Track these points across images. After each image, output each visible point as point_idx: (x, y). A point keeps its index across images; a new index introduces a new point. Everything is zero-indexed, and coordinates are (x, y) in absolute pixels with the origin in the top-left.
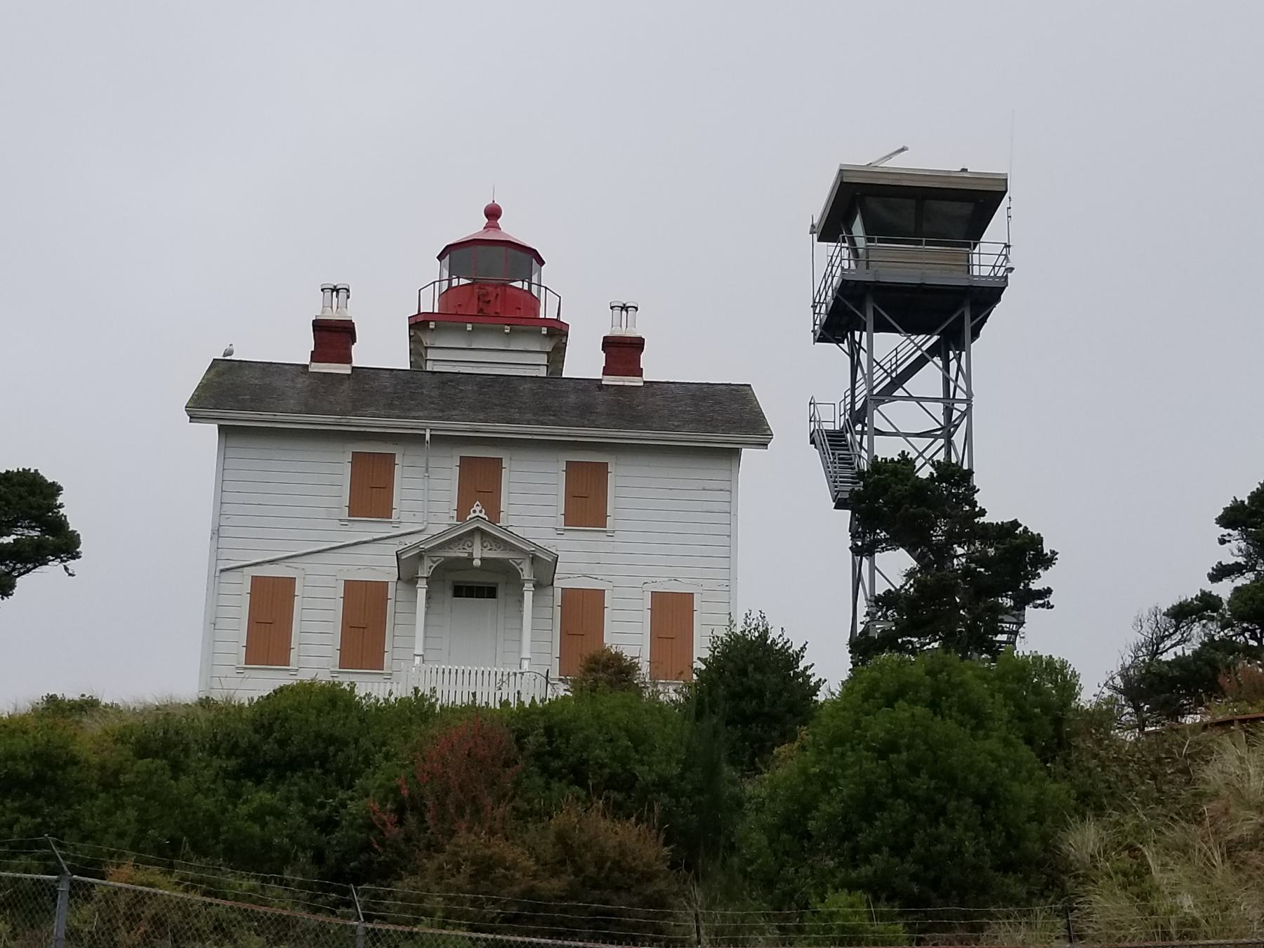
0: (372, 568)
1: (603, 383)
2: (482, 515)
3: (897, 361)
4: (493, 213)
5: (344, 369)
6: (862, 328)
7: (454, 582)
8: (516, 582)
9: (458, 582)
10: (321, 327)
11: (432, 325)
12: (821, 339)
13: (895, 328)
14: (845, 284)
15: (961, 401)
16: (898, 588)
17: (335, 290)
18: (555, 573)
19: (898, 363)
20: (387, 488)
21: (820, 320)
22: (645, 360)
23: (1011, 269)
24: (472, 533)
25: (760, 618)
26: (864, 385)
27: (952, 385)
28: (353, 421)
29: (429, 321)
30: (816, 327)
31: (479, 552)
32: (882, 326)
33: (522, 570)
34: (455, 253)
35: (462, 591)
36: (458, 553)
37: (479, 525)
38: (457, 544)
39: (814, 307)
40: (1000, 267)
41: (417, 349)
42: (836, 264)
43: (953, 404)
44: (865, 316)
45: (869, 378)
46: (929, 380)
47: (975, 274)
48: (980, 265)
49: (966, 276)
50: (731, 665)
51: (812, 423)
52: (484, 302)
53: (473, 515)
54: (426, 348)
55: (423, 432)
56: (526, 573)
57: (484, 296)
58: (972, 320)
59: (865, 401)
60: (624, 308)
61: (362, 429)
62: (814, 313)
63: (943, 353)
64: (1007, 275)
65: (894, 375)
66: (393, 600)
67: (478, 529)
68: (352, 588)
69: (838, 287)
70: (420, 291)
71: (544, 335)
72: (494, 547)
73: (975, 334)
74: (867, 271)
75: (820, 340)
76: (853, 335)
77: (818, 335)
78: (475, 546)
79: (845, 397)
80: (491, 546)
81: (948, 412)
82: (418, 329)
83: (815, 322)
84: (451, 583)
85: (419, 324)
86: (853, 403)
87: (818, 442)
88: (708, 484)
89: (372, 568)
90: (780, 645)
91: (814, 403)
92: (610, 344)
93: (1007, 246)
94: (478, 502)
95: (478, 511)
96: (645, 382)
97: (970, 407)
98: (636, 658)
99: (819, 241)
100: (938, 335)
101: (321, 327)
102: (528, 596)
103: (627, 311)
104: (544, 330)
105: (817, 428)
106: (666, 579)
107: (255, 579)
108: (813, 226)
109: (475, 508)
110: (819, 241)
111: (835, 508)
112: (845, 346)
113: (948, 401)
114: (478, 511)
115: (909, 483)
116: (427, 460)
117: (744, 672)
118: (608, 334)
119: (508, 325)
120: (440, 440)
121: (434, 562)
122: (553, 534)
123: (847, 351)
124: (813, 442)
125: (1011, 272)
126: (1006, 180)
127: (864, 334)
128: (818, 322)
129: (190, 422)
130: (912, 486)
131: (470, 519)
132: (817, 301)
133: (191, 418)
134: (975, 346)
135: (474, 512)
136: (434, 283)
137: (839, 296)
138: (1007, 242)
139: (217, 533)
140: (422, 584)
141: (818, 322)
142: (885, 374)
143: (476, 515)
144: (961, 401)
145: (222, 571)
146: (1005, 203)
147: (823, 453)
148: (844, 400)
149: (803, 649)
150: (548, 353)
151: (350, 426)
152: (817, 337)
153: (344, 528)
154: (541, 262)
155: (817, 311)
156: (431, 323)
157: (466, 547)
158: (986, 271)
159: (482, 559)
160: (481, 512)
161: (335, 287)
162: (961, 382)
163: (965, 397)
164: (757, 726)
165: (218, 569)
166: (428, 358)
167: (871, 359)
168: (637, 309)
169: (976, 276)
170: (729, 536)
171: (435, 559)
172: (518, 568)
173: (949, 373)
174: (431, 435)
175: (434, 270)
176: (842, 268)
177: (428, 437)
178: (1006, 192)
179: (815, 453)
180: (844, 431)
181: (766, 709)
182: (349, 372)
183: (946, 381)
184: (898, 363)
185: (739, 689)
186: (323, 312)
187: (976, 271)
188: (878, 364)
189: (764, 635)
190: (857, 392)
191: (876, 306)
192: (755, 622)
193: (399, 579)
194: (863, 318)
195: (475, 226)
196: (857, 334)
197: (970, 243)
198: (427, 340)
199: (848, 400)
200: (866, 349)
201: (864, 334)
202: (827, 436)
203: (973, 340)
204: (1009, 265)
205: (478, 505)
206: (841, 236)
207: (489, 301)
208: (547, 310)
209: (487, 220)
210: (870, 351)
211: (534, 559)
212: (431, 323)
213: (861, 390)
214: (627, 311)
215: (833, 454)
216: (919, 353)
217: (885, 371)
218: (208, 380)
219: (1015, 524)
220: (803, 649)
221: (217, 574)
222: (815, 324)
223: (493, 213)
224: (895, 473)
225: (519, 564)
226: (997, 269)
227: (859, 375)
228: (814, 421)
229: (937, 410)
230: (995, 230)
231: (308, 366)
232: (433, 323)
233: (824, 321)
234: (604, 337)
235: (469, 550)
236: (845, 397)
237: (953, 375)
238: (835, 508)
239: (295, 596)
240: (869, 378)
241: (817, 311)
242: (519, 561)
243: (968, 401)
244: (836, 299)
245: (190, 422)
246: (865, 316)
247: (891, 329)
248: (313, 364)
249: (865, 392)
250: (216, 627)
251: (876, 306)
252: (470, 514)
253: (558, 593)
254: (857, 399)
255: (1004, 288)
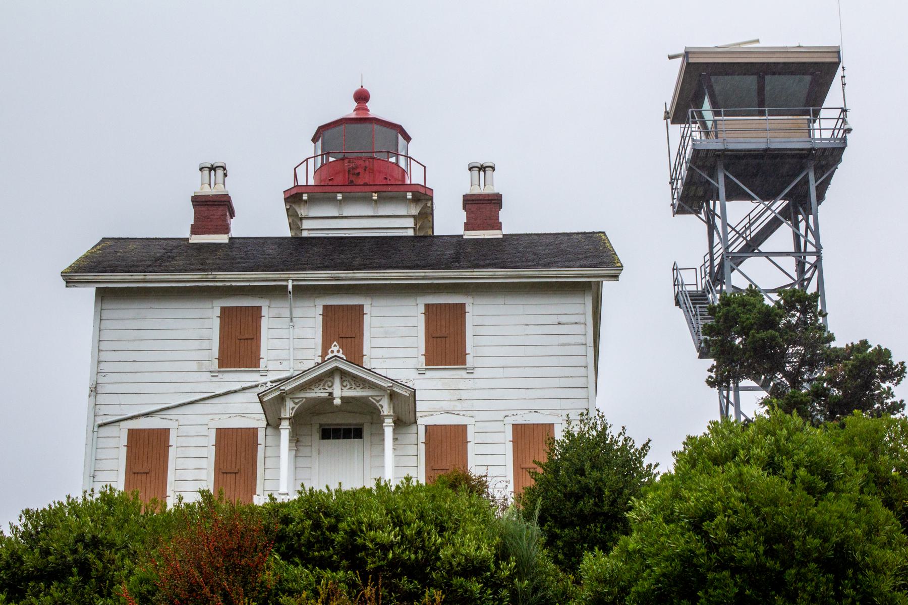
0: (242, 415)
1: (464, 237)
2: (340, 355)
3: (751, 233)
4: (362, 97)
5: (222, 239)
6: (715, 195)
7: (321, 425)
8: (377, 419)
9: (325, 425)
10: (199, 202)
11: (305, 197)
12: (680, 210)
13: (750, 195)
14: (696, 152)
15: (811, 254)
16: (742, 393)
17: (213, 168)
18: (415, 411)
19: (751, 222)
20: (254, 338)
21: (678, 193)
22: (503, 216)
23: (849, 130)
24: (331, 373)
25: (598, 418)
26: (720, 245)
27: (802, 240)
28: (218, 276)
29: (302, 193)
30: (675, 201)
31: (339, 391)
32: (734, 194)
33: (382, 407)
34: (328, 133)
35: (328, 433)
36: (318, 393)
37: (337, 365)
38: (317, 385)
39: (671, 183)
40: (839, 129)
41: (295, 220)
42: (688, 138)
43: (805, 258)
44: (718, 183)
45: (724, 240)
46: (782, 238)
47: (816, 137)
48: (820, 129)
49: (808, 139)
50: (566, 464)
51: (676, 287)
52: (354, 174)
53: (330, 355)
54: (301, 219)
55: (284, 283)
56: (386, 408)
57: (353, 169)
58: (816, 182)
59: (722, 258)
60: (482, 168)
61: (228, 284)
62: (672, 189)
63: (792, 217)
64: (845, 137)
65: (748, 238)
66: (263, 445)
67: (337, 369)
68: (223, 435)
69: (690, 158)
70: (295, 169)
71: (409, 199)
72: (354, 386)
73: (820, 198)
74: (717, 141)
75: (678, 212)
76: (708, 205)
77: (676, 207)
78: (334, 387)
79: (705, 263)
80: (351, 385)
81: (801, 266)
82: (294, 202)
83: (673, 195)
84: (318, 426)
85: (294, 198)
86: (712, 265)
87: (682, 302)
88: (564, 319)
89: (242, 415)
90: (620, 444)
91: (677, 269)
92: (469, 202)
93: (844, 111)
94: (335, 343)
95: (335, 351)
96: (504, 235)
97: (819, 258)
98: (484, 476)
99: (672, 123)
100: (784, 199)
101: (199, 202)
102: (389, 432)
103: (484, 171)
104: (409, 196)
105: (680, 289)
106: (527, 411)
107: (132, 433)
108: (667, 112)
109: (333, 348)
110: (672, 123)
111: (700, 357)
112: (703, 216)
113: (799, 253)
114: (335, 351)
115: (755, 311)
116: (291, 304)
117: (581, 472)
118: (468, 191)
119: (375, 192)
120: (302, 291)
121: (296, 404)
122: (413, 374)
123: (704, 219)
124: (678, 303)
125: (849, 133)
126: (839, 52)
127: (718, 203)
128: (676, 196)
129: (67, 286)
130: (759, 313)
131: (329, 359)
132: (673, 178)
133: (67, 282)
134: (824, 210)
135: (332, 352)
136: (307, 160)
137: (692, 166)
138: (843, 106)
139: (94, 391)
140: (285, 424)
141: (676, 196)
142: (737, 235)
143: (333, 355)
144: (811, 254)
145: (100, 426)
146: (839, 72)
147: (687, 312)
148: (704, 264)
149: (646, 446)
150: (414, 216)
151: (217, 281)
152: (675, 210)
153: (214, 379)
154: (408, 138)
155: (674, 187)
156: (304, 195)
157: (326, 388)
158: (827, 134)
159: (342, 398)
160: (338, 351)
161: (212, 166)
162: (810, 237)
163: (814, 250)
164: (595, 526)
165: (96, 424)
166: (303, 228)
167: (725, 224)
168: (493, 168)
169: (818, 139)
170: (586, 367)
171: (297, 401)
172: (378, 404)
173: (799, 230)
174: (293, 286)
175: (310, 149)
176: (693, 140)
177: (290, 288)
178: (839, 62)
179: (680, 312)
180: (706, 291)
181: (606, 508)
182: (227, 241)
183: (797, 237)
184: (751, 222)
185: (576, 488)
186: (202, 189)
187: (817, 135)
188: (733, 229)
189: (602, 434)
190: (715, 250)
191: (728, 174)
192: (593, 421)
193: (268, 425)
194: (716, 184)
195: (349, 109)
196: (711, 203)
197: (809, 110)
198: (302, 211)
199: (708, 264)
200: (720, 215)
201: (718, 203)
202: (690, 296)
203: (819, 203)
204: (847, 127)
205: (335, 346)
206: (690, 110)
207: (358, 174)
208: (416, 177)
209: (356, 104)
210: (724, 217)
211: (393, 396)
212: (304, 195)
213: (719, 249)
214: (484, 171)
215: (694, 307)
216: (773, 215)
217: (737, 232)
218: (92, 253)
219: (864, 344)
220: (646, 446)
221: (96, 429)
222: (673, 199)
223: (362, 97)
224: (743, 304)
225: (378, 401)
226: (836, 131)
227: (716, 240)
228: (678, 285)
229: (790, 264)
230: (833, 98)
231: (188, 238)
232: (306, 195)
233: (680, 194)
234: (464, 196)
235: (330, 390)
236: (705, 263)
237: (802, 231)
238: (700, 357)
239: (169, 446)
240: (724, 240)
241: (674, 187)
242: (378, 398)
243: (818, 253)
244: (690, 170)
245: (67, 286)
246: (718, 183)
247: (746, 197)
248: (193, 236)
249: (721, 251)
250: (96, 479)
251: (728, 174)
252: (328, 354)
253: (422, 430)
254: (715, 257)
255: (843, 149)
